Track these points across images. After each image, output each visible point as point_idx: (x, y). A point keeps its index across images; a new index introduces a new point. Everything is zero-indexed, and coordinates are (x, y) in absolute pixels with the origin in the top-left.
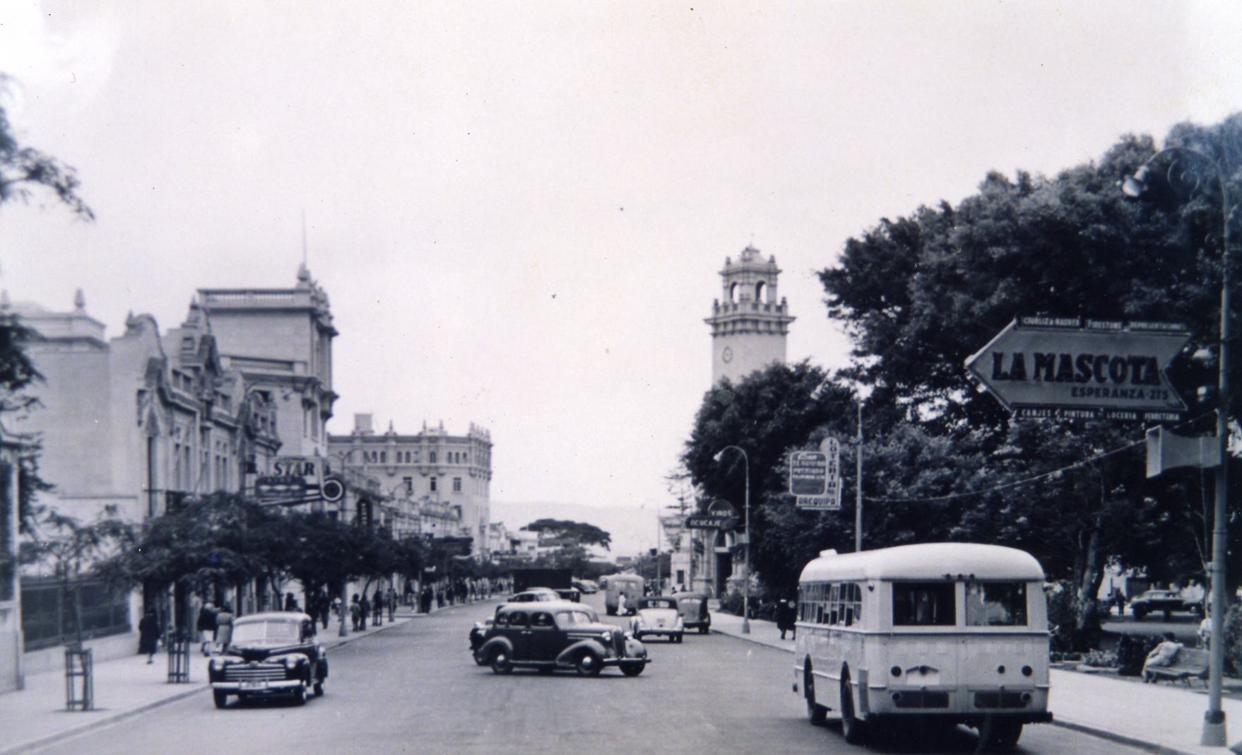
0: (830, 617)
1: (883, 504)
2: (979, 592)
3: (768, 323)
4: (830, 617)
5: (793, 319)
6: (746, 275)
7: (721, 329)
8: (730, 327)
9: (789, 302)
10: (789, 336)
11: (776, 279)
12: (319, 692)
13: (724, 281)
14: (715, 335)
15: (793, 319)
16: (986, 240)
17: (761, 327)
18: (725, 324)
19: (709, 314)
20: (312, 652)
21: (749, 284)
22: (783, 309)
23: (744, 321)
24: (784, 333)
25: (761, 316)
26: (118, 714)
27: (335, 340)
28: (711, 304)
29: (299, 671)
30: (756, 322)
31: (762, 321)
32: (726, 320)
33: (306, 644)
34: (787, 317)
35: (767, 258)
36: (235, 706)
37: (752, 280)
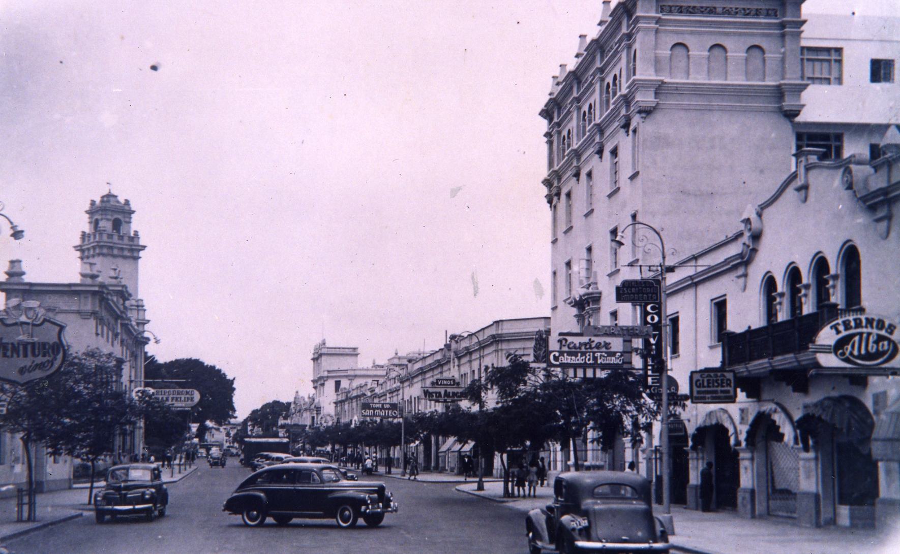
0: (727, 395)
1: (335, 424)
2: (533, 476)
3: (122, 249)
4: (727, 395)
5: (144, 247)
6: (104, 213)
7: (86, 253)
8: (92, 252)
9: (140, 234)
10: (140, 261)
11: (130, 218)
12: (162, 514)
13: (89, 218)
14: (82, 258)
15: (144, 247)
16: (688, 403)
17: (116, 252)
18: (88, 249)
19: (78, 242)
20: (159, 488)
21: (108, 220)
22: (135, 239)
23: (101, 247)
24: (137, 258)
25: (114, 243)
26: (46, 523)
27: (146, 312)
28: (79, 235)
29: (152, 500)
30: (111, 248)
31: (116, 248)
32: (89, 246)
33: (157, 482)
34: (139, 246)
35: (122, 201)
36: (109, 522)
37: (109, 217)
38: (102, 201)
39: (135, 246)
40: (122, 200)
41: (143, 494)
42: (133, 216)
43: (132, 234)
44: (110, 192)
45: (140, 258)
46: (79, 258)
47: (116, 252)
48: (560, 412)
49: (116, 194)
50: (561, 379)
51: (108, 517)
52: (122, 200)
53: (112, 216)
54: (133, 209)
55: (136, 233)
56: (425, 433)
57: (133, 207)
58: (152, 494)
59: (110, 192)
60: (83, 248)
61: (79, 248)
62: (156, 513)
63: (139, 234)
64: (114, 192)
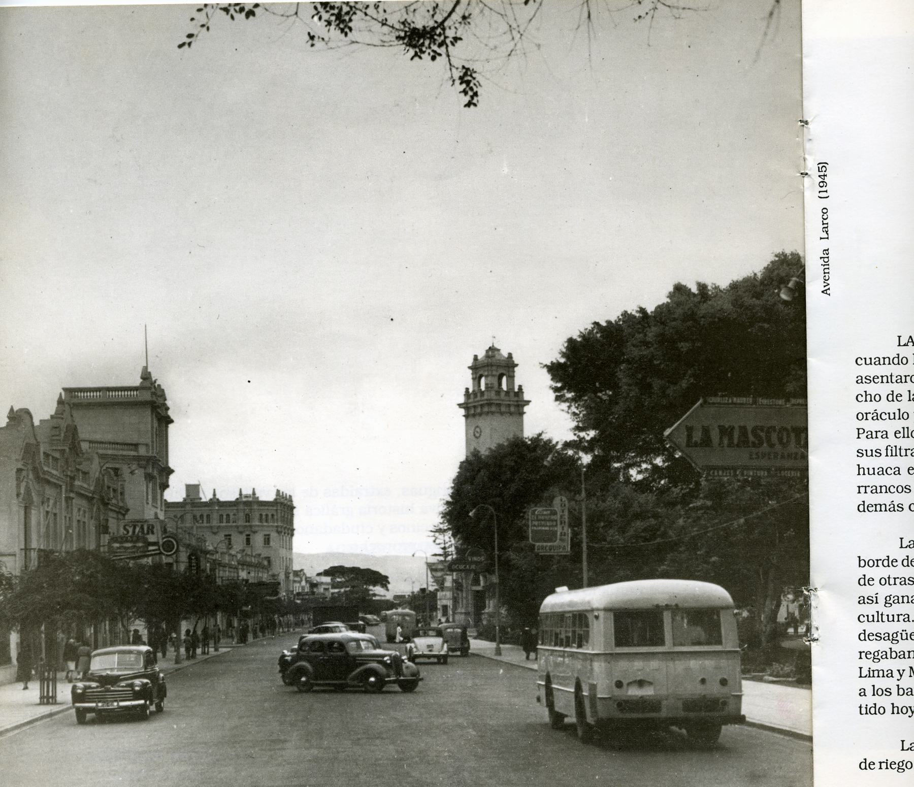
7: (472, 412)
8: (479, 410)
9: (524, 389)
11: (514, 372)
12: (160, 709)
14: (466, 416)
17: (503, 409)
18: (475, 407)
19: (462, 400)
24: (522, 414)
30: (499, 405)
35: (506, 355)
36: (93, 722)
37: (494, 373)
38: (487, 356)
39: (521, 401)
40: (505, 354)
41: (132, 686)
42: (516, 369)
43: (516, 390)
44: (493, 346)
45: (525, 413)
46: (464, 416)
47: (503, 409)
48: (618, 462)
49: (499, 348)
50: (782, 286)
51: (89, 716)
52: (505, 354)
53: (497, 371)
54: (516, 362)
55: (520, 387)
56: (43, 628)
57: (516, 360)
58: (145, 685)
59: (493, 346)
60: (469, 405)
61: (464, 406)
62: (153, 708)
63: (523, 388)
64: (497, 346)
